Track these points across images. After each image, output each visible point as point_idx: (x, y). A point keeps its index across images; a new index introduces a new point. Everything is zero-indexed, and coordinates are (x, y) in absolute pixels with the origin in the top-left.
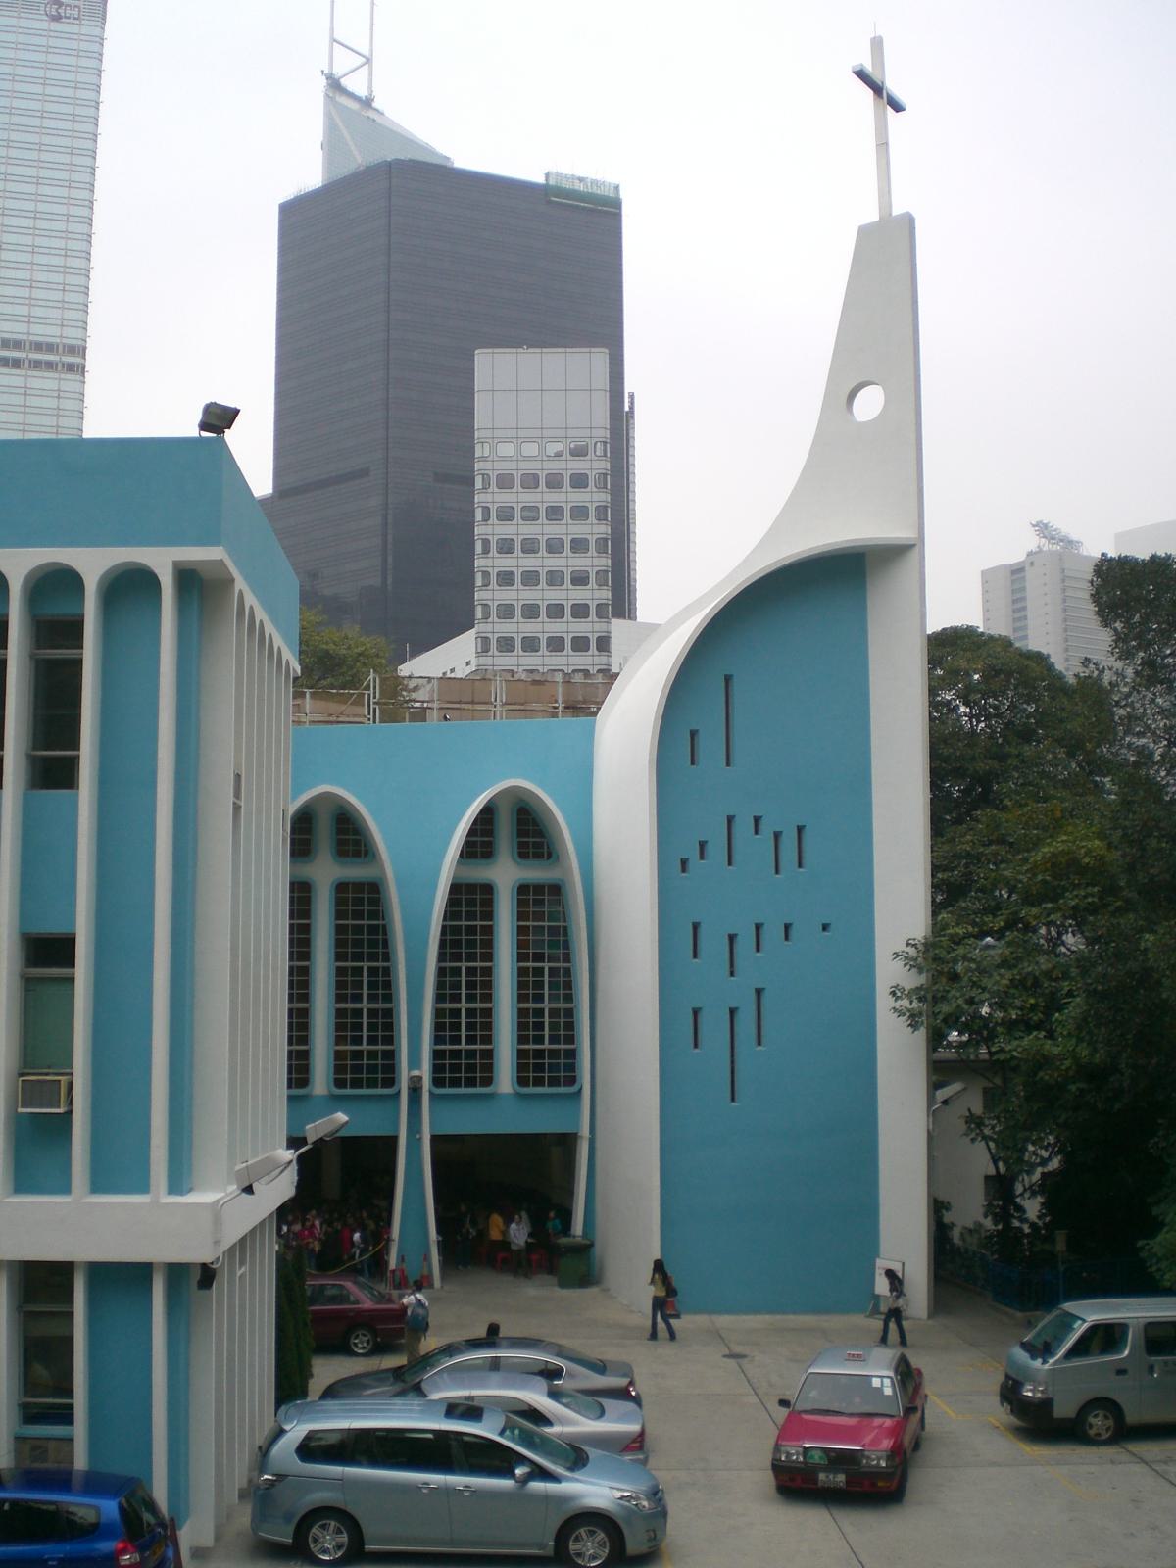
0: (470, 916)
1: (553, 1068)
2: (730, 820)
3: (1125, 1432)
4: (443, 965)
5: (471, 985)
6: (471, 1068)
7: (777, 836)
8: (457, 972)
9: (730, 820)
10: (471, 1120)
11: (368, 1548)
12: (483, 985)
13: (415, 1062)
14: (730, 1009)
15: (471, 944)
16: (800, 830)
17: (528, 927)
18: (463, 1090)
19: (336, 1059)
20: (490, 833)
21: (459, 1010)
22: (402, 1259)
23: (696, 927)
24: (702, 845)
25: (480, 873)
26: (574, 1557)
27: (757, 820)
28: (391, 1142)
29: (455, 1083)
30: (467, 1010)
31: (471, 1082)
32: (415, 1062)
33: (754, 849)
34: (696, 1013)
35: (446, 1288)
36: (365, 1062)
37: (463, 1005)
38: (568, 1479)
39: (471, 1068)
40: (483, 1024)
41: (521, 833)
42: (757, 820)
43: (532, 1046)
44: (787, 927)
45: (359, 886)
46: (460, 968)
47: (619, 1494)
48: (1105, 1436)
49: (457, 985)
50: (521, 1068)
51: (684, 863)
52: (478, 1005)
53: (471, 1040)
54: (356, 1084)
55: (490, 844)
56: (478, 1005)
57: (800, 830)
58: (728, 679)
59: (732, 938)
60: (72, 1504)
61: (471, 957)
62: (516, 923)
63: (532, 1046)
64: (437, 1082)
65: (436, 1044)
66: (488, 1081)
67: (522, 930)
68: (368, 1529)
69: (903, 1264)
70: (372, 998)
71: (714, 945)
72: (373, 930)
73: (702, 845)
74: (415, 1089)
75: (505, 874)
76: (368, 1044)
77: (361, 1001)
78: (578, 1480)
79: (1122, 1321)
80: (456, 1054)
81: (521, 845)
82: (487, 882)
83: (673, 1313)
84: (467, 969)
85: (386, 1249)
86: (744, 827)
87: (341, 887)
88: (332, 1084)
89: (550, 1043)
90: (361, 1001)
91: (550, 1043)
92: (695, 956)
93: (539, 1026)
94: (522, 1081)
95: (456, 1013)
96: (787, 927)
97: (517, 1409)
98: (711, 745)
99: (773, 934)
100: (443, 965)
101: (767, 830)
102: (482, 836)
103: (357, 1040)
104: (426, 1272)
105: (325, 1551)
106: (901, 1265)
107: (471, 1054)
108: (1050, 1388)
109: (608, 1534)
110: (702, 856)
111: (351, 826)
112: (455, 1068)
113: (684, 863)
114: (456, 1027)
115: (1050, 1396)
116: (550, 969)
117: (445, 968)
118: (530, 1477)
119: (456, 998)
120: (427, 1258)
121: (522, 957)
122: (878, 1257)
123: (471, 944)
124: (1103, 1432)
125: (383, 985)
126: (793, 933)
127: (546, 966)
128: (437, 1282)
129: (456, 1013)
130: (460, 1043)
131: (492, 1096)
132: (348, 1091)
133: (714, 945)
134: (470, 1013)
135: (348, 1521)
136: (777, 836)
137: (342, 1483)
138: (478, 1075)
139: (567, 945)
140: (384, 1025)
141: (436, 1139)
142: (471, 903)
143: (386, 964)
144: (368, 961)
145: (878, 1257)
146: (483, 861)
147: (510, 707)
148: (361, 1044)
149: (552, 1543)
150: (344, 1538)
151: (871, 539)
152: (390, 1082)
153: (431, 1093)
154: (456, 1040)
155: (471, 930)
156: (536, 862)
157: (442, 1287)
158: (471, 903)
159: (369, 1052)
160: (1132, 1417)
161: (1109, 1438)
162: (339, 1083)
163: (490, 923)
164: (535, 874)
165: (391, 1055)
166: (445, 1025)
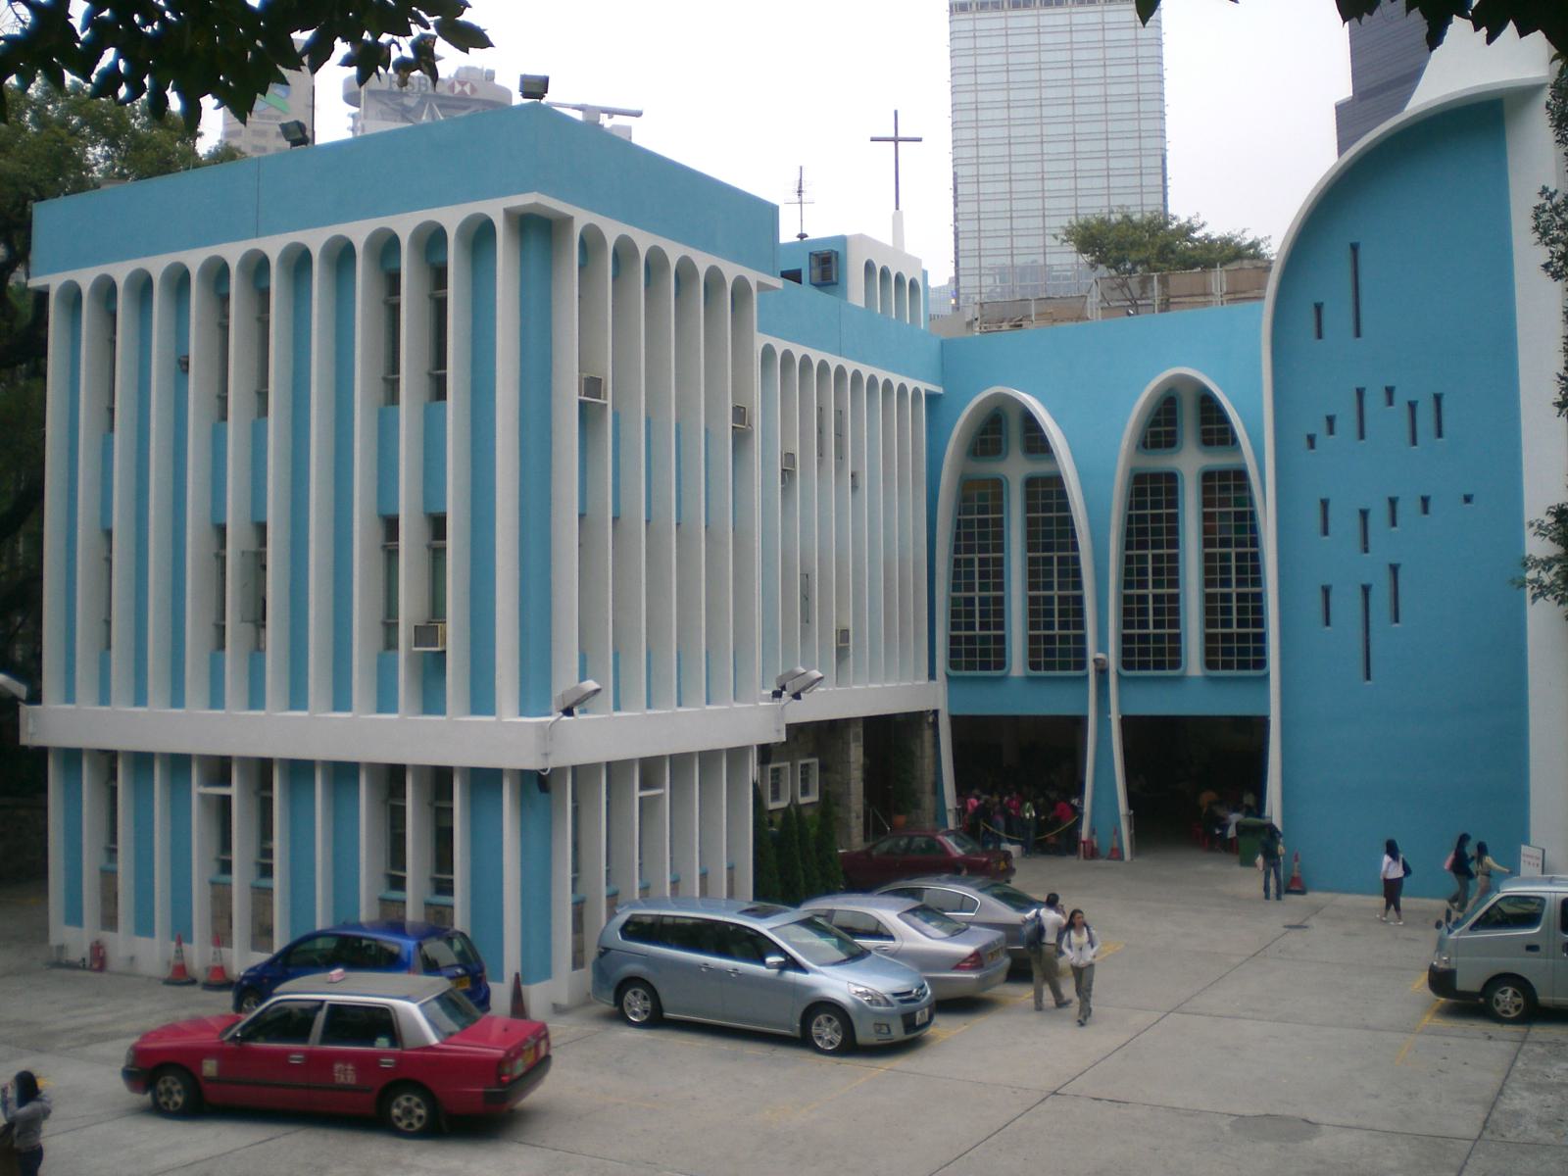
0: (1156, 505)
1: (1242, 651)
2: (1360, 393)
3: (1535, 1012)
4: (1130, 552)
5: (1157, 571)
6: (1160, 652)
7: (1412, 406)
8: (1143, 559)
9: (1360, 393)
10: (1158, 701)
11: (668, 1015)
12: (1169, 571)
13: (1102, 647)
14: (1323, 587)
15: (1157, 532)
16: (1438, 398)
17: (1214, 513)
18: (1058, 673)
19: (952, 643)
20: (1173, 422)
21: (973, 599)
22: (1093, 831)
23: (1325, 504)
24: (1330, 420)
25: (1160, 462)
26: (815, 1039)
27: (1390, 391)
28: (1080, 722)
29: (1144, 666)
30: (980, 598)
31: (1159, 665)
32: (1102, 647)
33: (1386, 422)
34: (1326, 591)
35: (1135, 861)
36: (1057, 646)
37: (1150, 591)
38: (815, 971)
39: (1242, 651)
40: (1169, 609)
41: (1204, 420)
42: (1390, 391)
43: (1136, 631)
44: (1425, 501)
45: (1224, 475)
46: (1052, 558)
47: (854, 989)
48: (1513, 1014)
49: (1143, 572)
50: (1033, 653)
51: (1311, 441)
52: (1165, 591)
53: (984, 626)
54: (1050, 666)
55: (1173, 434)
56: (1165, 591)
57: (1438, 398)
58: (1355, 248)
59: (1364, 514)
60: (389, 942)
61: (1157, 545)
62: (1180, 511)
63: (1136, 631)
64: (1127, 665)
65: (1124, 628)
66: (1001, 665)
67: (1207, 517)
68: (665, 999)
69: (1544, 851)
70: (983, 587)
71: (1344, 522)
72: (1240, 516)
73: (1330, 420)
74: (1102, 672)
75: (1189, 462)
76: (1059, 629)
77: (1230, 586)
78: (822, 973)
79: (1539, 894)
80: (1144, 638)
81: (1204, 433)
82: (1170, 470)
83: (1297, 888)
84: (1154, 556)
85: (1078, 824)
86: (1375, 401)
87: (1208, 477)
88: (1120, 665)
89: (1155, 628)
90: (1230, 586)
91: (1155, 628)
92: (1325, 532)
93: (1227, 611)
94: (1210, 664)
95: (1143, 599)
96: (1425, 501)
97: (845, 925)
98: (1338, 318)
99: (1408, 508)
100: (1130, 552)
101: (1401, 400)
102: (1166, 425)
103: (1049, 626)
104: (1116, 845)
105: (635, 1014)
106: (1541, 851)
107: (1159, 638)
108: (1453, 959)
109: (841, 1022)
110: (1331, 431)
111: (1215, 415)
112: (1144, 652)
113: (1311, 441)
114: (1143, 612)
115: (1453, 967)
116: (980, 559)
117: (1132, 556)
118: (782, 967)
119: (1143, 585)
120: (1117, 832)
121: (1207, 543)
122: (1527, 843)
123: (1157, 532)
124: (1512, 1010)
125: (1071, 573)
126: (1432, 507)
127: (1055, 555)
128: (1127, 856)
129: (1143, 599)
130: (974, 630)
131: (1181, 679)
132: (1042, 673)
133: (1344, 522)
134: (1157, 598)
135: (653, 994)
136: (1412, 406)
137: (648, 959)
138: (1167, 658)
139: (1254, 529)
140: (1074, 610)
141: (1126, 722)
142: (1156, 492)
143: (1253, 550)
144: (1058, 550)
145: (1527, 843)
146: (1169, 450)
147: (1232, 296)
148: (1053, 629)
149: (798, 1025)
150: (648, 1005)
151: (1446, 96)
152: (1081, 665)
153: (1120, 677)
154: (1144, 624)
155: (1156, 518)
156: (1221, 448)
157: (1132, 859)
158: (1156, 492)
159: (1061, 636)
160: (1544, 998)
161: (1516, 1017)
162: (1034, 666)
163: (1206, 510)
164: (1219, 460)
165: (1081, 639)
166: (1132, 609)
